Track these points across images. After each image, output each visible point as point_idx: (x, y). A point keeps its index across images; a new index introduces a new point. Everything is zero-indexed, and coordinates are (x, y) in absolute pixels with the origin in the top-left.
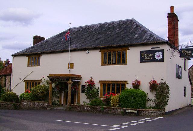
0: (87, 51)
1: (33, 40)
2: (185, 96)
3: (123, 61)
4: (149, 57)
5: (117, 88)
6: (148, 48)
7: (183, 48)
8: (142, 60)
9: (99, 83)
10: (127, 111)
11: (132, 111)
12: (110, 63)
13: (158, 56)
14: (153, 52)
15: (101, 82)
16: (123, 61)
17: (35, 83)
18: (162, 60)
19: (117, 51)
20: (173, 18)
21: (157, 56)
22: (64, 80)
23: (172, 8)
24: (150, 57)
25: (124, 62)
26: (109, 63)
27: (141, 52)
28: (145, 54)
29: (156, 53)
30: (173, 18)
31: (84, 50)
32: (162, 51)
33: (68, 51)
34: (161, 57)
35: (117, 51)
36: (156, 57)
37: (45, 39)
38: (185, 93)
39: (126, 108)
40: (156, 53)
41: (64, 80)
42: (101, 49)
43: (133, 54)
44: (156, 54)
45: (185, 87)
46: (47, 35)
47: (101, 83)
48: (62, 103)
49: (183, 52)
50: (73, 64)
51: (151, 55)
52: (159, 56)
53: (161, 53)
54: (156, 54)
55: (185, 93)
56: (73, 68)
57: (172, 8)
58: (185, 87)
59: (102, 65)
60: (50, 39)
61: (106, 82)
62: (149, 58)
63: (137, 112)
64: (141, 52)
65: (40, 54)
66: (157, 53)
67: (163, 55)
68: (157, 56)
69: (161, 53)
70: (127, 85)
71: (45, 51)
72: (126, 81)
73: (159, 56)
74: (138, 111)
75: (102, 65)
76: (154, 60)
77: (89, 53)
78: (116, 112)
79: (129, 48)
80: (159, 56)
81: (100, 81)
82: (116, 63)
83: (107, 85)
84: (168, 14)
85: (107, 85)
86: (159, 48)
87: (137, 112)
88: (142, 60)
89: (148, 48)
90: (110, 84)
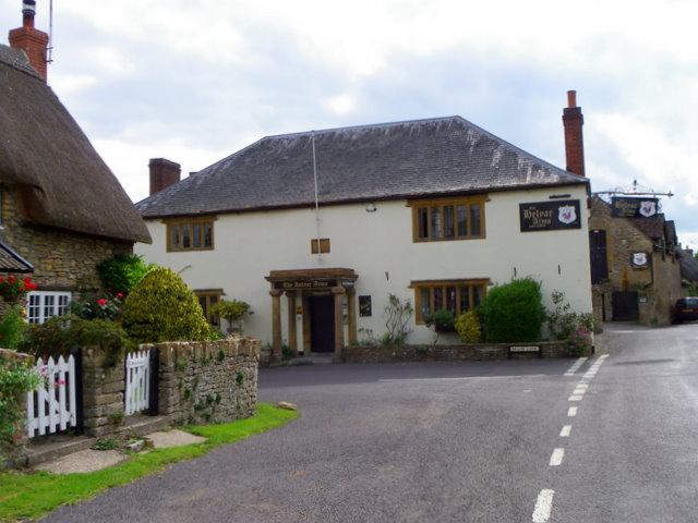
0: (371, 207)
1: (147, 170)
3: (472, 227)
6: (543, 197)
7: (618, 195)
8: (526, 226)
9: (411, 287)
10: (512, 349)
11: (526, 349)
14: (552, 207)
16: (472, 227)
17: (208, 299)
20: (573, 119)
21: (564, 215)
22: (322, 284)
23: (572, 95)
25: (208, 244)
26: (460, 234)
27: (523, 207)
30: (573, 119)
34: (573, 217)
36: (561, 218)
37: (184, 175)
41: (322, 284)
43: (501, 214)
44: (562, 210)
46: (193, 160)
48: (300, 347)
49: (617, 205)
53: (573, 209)
54: (562, 210)
56: (328, 251)
57: (572, 95)
60: (213, 171)
63: (537, 349)
64: (523, 207)
65: (214, 215)
68: (564, 215)
69: (573, 209)
71: (225, 207)
73: (568, 216)
74: (540, 347)
76: (556, 225)
79: (490, 197)
80: (568, 216)
84: (565, 110)
86: (569, 196)
87: (537, 349)
88: (526, 226)
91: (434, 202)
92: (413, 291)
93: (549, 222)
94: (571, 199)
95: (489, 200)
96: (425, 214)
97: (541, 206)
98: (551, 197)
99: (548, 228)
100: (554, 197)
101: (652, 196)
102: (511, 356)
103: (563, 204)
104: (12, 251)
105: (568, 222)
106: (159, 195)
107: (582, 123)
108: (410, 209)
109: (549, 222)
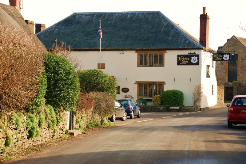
2: (212, 94)
3: (159, 62)
4: (220, 57)
5: (144, 89)
8: (179, 63)
9: (135, 84)
10: (170, 108)
11: (175, 108)
12: (146, 65)
13: (194, 59)
14: (189, 56)
15: (138, 83)
16: (159, 62)
18: (198, 64)
19: (144, 54)
20: (204, 18)
23: (204, 9)
24: (187, 61)
27: (179, 56)
28: (182, 58)
29: (224, 55)
30: (204, 18)
31: (118, 50)
32: (198, 56)
33: (99, 50)
34: (197, 61)
35: (144, 54)
36: (192, 61)
38: (212, 92)
39: (169, 105)
40: (224, 55)
42: (137, 50)
43: (171, 57)
44: (192, 58)
45: (213, 86)
47: (138, 84)
50: (104, 64)
51: (221, 56)
52: (227, 58)
53: (197, 57)
54: (192, 58)
55: (212, 92)
57: (204, 9)
58: (213, 86)
59: (138, 66)
61: (143, 83)
62: (186, 62)
63: (179, 108)
64: (179, 56)
66: (225, 55)
67: (198, 59)
68: (193, 60)
69: (197, 57)
70: (164, 85)
72: (164, 82)
74: (180, 107)
75: (138, 66)
76: (190, 63)
77: (123, 53)
78: (159, 109)
79: (167, 51)
81: (136, 82)
82: (153, 65)
83: (143, 85)
84: (201, 15)
85: (143, 85)
87: (179, 108)
88: (179, 63)
89: (186, 53)
90: (147, 85)
91: (146, 52)
92: (136, 85)
93: (188, 62)
94: (196, 54)
95: (167, 53)
96: (142, 57)
97: (185, 56)
98: (188, 53)
99: (187, 64)
100: (190, 53)
101: (228, 53)
102: (169, 110)
103: (193, 56)
104: (238, 125)
105: (194, 63)
106: (24, 21)
107: (168, 91)
108: (137, 54)
109: (188, 62)
